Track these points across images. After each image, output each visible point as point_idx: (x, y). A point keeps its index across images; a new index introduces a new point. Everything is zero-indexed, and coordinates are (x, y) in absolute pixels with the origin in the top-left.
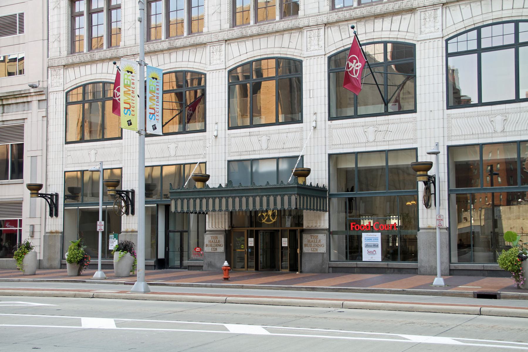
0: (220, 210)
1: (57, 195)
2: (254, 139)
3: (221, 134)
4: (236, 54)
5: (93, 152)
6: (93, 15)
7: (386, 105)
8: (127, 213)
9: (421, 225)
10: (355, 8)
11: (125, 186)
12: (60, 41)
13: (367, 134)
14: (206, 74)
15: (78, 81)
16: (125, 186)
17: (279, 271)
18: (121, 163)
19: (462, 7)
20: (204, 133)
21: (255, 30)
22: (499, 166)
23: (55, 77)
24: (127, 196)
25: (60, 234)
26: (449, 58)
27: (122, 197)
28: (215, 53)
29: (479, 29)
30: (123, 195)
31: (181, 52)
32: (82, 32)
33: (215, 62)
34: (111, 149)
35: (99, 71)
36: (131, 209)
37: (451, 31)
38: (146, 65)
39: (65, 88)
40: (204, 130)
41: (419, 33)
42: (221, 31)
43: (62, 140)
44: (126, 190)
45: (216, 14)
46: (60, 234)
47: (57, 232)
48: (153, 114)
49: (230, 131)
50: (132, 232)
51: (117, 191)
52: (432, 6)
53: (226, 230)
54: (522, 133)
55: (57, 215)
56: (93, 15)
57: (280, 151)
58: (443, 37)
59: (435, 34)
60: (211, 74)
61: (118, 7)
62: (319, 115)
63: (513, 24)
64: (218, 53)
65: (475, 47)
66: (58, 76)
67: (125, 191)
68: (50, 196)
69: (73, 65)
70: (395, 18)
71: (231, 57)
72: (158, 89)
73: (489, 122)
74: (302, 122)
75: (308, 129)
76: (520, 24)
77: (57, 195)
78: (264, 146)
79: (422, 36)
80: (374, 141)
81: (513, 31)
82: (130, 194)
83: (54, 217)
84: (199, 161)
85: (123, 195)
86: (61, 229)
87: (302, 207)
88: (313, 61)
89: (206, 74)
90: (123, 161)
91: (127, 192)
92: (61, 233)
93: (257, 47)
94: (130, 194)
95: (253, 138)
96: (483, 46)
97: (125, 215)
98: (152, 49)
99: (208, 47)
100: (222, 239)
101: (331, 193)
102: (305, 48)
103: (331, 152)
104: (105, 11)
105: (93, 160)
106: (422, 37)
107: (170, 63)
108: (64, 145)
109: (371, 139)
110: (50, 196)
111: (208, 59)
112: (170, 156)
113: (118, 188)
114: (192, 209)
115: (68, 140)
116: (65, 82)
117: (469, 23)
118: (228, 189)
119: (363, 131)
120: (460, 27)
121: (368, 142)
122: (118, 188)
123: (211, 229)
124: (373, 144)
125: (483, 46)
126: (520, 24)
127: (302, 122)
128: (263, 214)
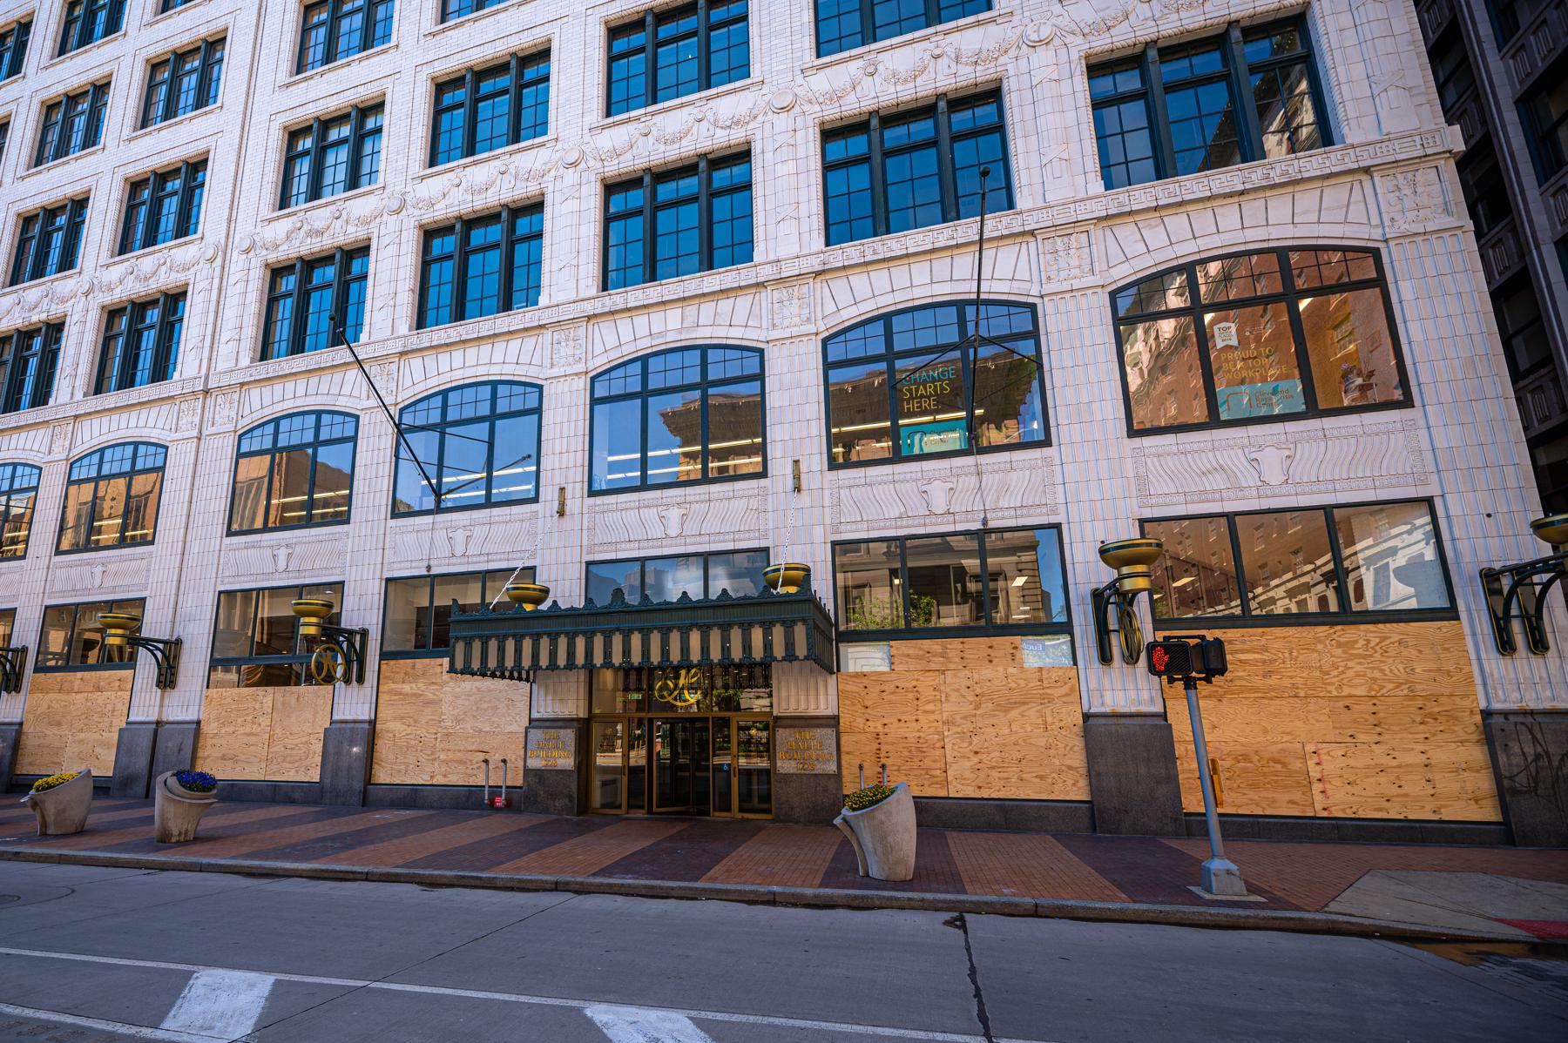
1: (364, 633)
2: (650, 514)
4: (418, 376)
8: (347, 681)
13: (452, 542)
14: (763, 350)
15: (267, 411)
17: (709, 815)
18: (533, 555)
19: (1271, 203)
20: (151, 547)
22: (897, 582)
24: (351, 644)
26: (830, 372)
28: (563, 344)
34: (751, 500)
35: (498, 358)
39: (399, 400)
40: (763, 474)
41: (549, 366)
45: (567, 269)
49: (395, 520)
52: (1417, 161)
53: (578, 720)
54: (618, 547)
55: (361, 680)
57: (641, 545)
58: (817, 334)
63: (698, 352)
65: (487, 412)
68: (161, 646)
71: (247, 411)
73: (1246, 464)
75: (548, 514)
76: (323, 416)
77: (364, 633)
79: (553, 370)
80: (680, 535)
81: (698, 362)
83: (354, 683)
84: (520, 565)
85: (341, 639)
89: (763, 350)
90: (150, 586)
91: (351, 633)
95: (645, 513)
97: (343, 685)
99: (177, 402)
102: (547, 362)
106: (556, 372)
107: (1243, 228)
108: (224, 538)
109: (939, 505)
110: (161, 646)
115: (596, 487)
116: (590, 357)
119: (1243, 459)
124: (284, 575)
126: (323, 416)
128: (669, 682)
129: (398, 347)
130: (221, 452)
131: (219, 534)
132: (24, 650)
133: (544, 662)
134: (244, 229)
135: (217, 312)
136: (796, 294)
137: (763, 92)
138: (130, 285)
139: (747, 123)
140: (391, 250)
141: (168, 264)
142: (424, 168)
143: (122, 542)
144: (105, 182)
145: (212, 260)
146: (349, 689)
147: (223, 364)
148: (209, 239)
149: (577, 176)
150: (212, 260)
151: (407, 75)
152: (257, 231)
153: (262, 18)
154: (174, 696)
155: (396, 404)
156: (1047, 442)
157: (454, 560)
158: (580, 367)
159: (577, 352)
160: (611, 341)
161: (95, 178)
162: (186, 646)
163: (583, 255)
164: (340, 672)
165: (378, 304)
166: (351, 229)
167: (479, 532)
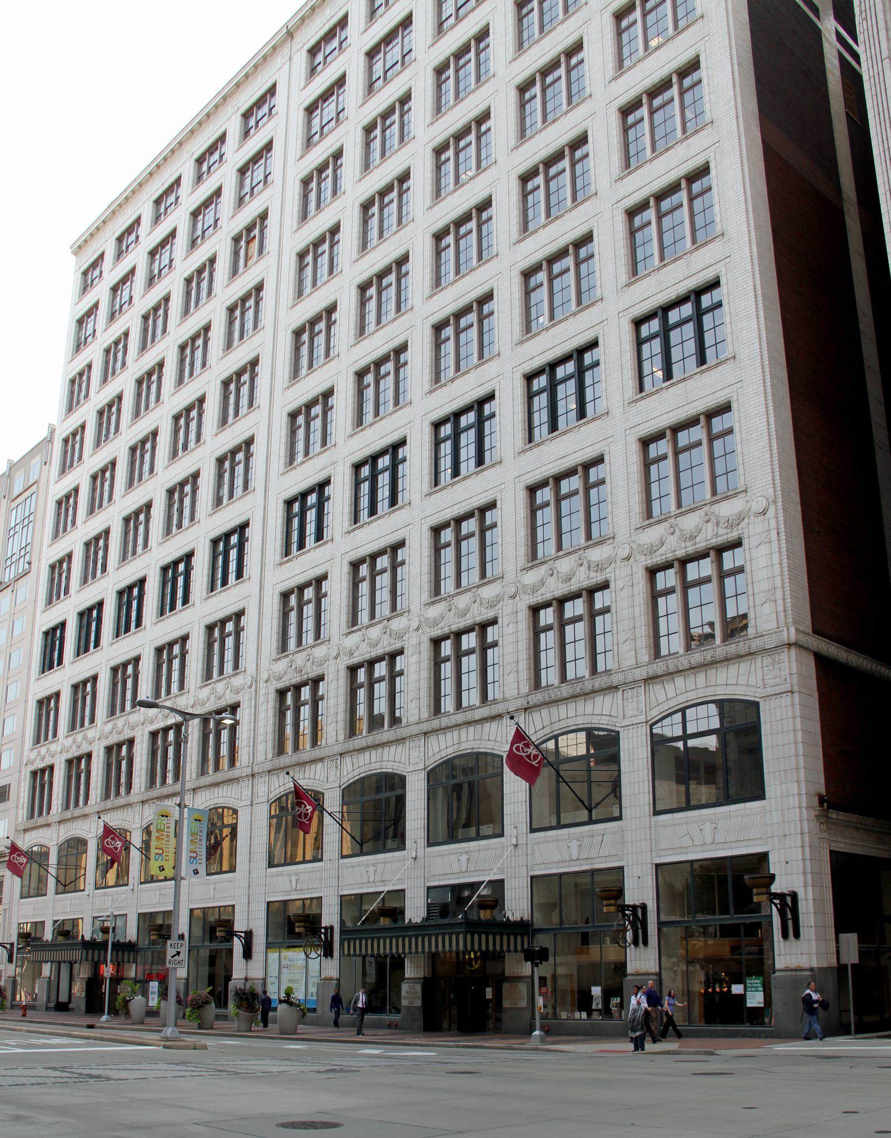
0: (516, 951)
3: (522, 840)
5: (464, 858)
6: (659, 600)
7: (590, 811)
8: (635, 943)
9: (778, 966)
10: (682, 656)
11: (630, 898)
12: (635, 639)
15: (673, 703)
16: (630, 898)
20: (620, 822)
21: (370, 740)
23: (630, 700)
24: (635, 914)
25: (335, 982)
27: (627, 915)
29: (683, 711)
30: (627, 912)
31: (692, 677)
32: (362, 710)
33: (630, 714)
35: (572, 713)
36: (640, 939)
37: (655, 713)
38: (185, 806)
39: (649, 718)
42: (638, 666)
43: (647, 809)
44: (632, 903)
45: (628, 642)
46: (655, 977)
47: (331, 979)
48: (195, 858)
50: (796, 970)
51: (619, 906)
55: (645, 943)
56: (659, 600)
59: (782, 686)
60: (626, 732)
61: (495, 644)
62: (520, 827)
64: (635, 699)
66: (776, 666)
67: (629, 906)
69: (538, 706)
70: (485, 725)
71: (431, 754)
72: (201, 831)
74: (764, 798)
77: (644, 907)
78: (709, 840)
82: (640, 911)
84: (487, 879)
85: (627, 912)
86: (653, 967)
87: (401, 950)
88: (774, 702)
91: (634, 908)
92: (655, 974)
93: (580, 710)
94: (640, 911)
96: (689, 732)
97: (632, 946)
98: (553, 697)
100: (418, 988)
101: (536, 926)
103: (658, 861)
104: (453, 659)
105: (372, 879)
106: (627, 722)
108: (652, 818)
110: (243, 935)
111: (620, 708)
112: (704, 844)
113: (619, 902)
114: (369, 952)
117: (674, 703)
118: (432, 922)
120: (665, 708)
121: (704, 844)
122: (619, 902)
123: (412, 976)
125: (689, 732)
127: (764, 798)
129: (641, 673)
130: (262, 814)
131: (524, 831)
132: (332, 928)
133: (413, 950)
134: (265, 664)
135: (255, 722)
136: (777, 659)
137: (615, 544)
138: (476, 612)
139: (738, 524)
140: (625, 593)
141: (311, 660)
142: (528, 562)
143: (117, 885)
144: (65, 685)
145: (250, 687)
146: (787, 943)
147: (260, 758)
148: (248, 671)
149: (629, 567)
150: (250, 687)
151: (338, 560)
152: (633, 539)
153: (886, 179)
154: (251, 963)
155: (647, 722)
156: (619, 818)
157: (370, 885)
158: (642, 718)
159: (783, 673)
160: (662, 697)
161: (190, 625)
162: (254, 933)
163: (520, 664)
164: (629, 935)
165: (330, 721)
166: (721, 531)
167: (380, 867)
